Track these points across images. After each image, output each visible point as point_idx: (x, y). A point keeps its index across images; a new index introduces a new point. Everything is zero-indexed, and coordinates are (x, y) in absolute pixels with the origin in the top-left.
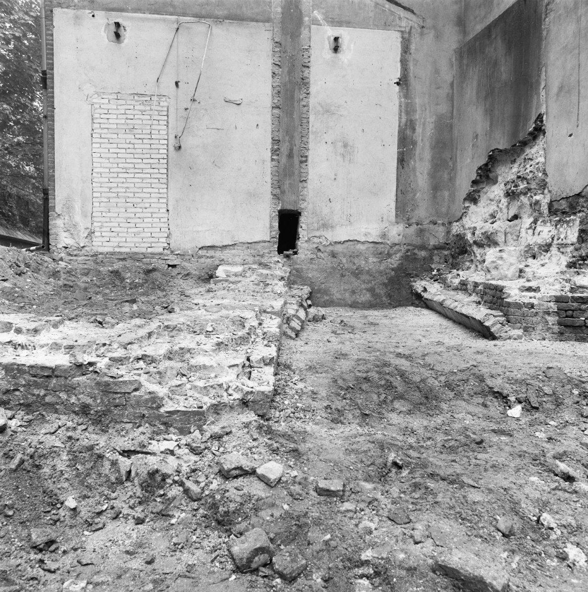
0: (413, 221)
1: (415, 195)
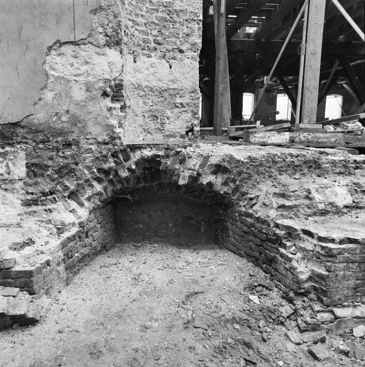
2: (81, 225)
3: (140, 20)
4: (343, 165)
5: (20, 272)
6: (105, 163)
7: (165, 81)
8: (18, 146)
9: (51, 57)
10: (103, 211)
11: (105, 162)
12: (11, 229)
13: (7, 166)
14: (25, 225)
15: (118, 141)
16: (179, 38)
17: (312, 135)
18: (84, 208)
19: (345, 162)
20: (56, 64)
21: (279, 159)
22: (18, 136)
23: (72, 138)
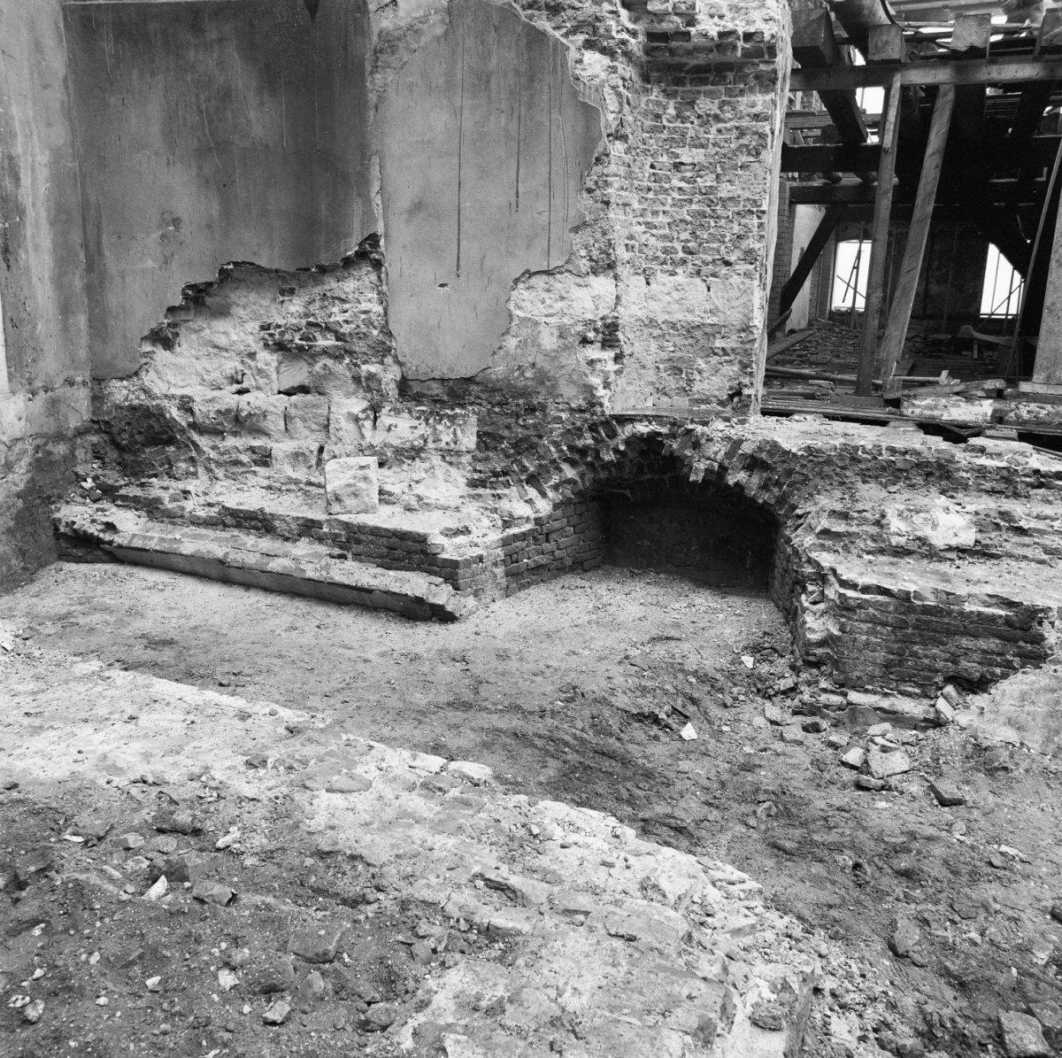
0: (38, 384)
1: (34, 327)
2: (538, 521)
3: (662, 219)
4: (1003, 478)
5: (446, 560)
6: (579, 438)
7: (697, 313)
8: (470, 408)
10: (580, 508)
11: (580, 437)
12: (448, 513)
14: (464, 510)
15: (598, 409)
16: (724, 242)
17: (1049, 407)
19: (1009, 471)
21: (865, 456)
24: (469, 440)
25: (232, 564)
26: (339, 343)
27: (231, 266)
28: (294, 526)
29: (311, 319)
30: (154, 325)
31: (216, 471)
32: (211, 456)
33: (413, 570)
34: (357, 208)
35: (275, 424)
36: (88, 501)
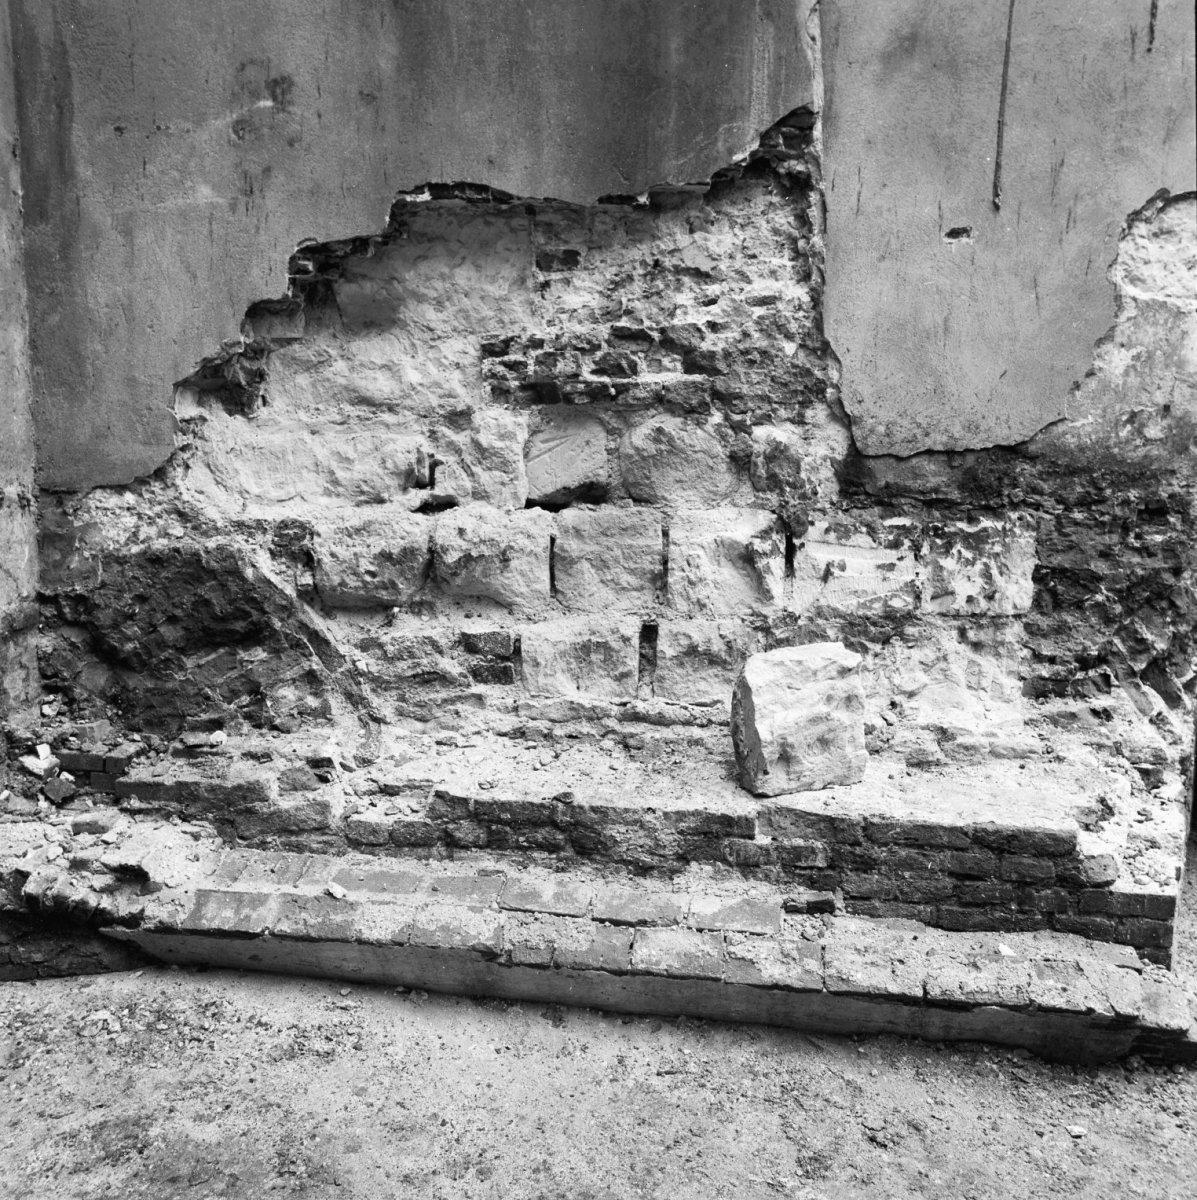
8: (1014, 516)
9: (1131, 244)
12: (1030, 764)
13: (987, 575)
18: (1180, 711)
20: (1146, 263)
22: (1015, 486)
23: (1170, 490)
24: (1019, 591)
25: (519, 957)
26: (697, 378)
27: (426, 196)
28: (668, 836)
29: (624, 322)
30: (211, 350)
31: (375, 701)
32: (361, 665)
33: (1035, 928)
34: (761, 47)
35: (527, 578)
36: (43, 804)
